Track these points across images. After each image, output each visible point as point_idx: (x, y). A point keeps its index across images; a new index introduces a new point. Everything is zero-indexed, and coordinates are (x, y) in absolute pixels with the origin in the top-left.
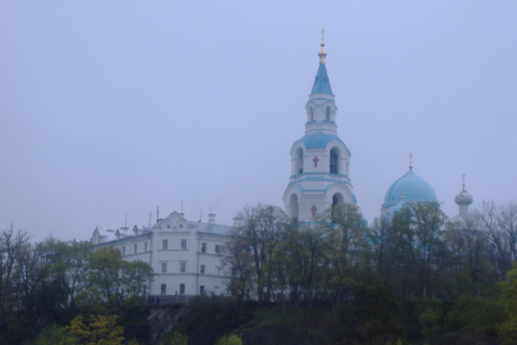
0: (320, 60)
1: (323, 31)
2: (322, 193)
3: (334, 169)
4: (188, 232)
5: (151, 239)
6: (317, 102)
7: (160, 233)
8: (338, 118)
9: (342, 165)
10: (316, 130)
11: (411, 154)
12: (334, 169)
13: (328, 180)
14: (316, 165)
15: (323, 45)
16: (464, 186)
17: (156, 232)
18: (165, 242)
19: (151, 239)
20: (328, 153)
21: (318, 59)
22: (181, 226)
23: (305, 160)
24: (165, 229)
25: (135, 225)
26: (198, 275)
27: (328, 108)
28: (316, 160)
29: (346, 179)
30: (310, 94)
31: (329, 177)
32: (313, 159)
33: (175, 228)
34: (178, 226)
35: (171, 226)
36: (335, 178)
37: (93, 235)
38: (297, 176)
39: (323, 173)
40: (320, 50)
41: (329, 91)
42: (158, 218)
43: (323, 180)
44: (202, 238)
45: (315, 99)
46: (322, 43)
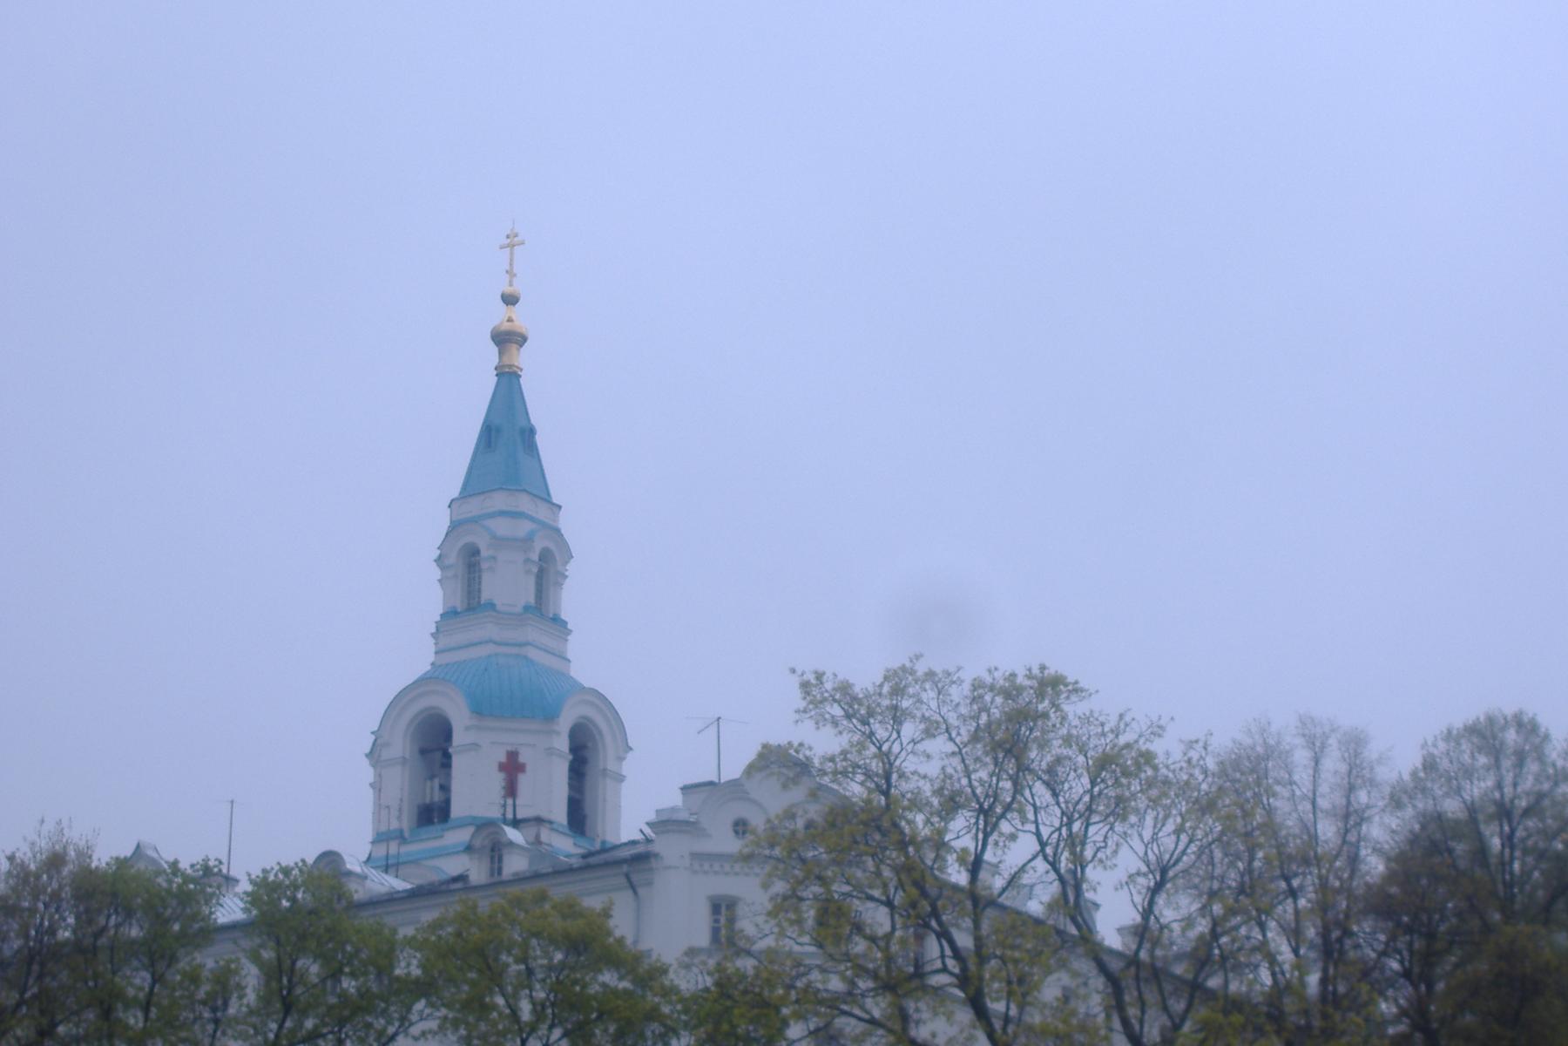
0: (497, 360)
1: (512, 242)
5: (635, 893)
6: (502, 527)
7: (696, 856)
8: (572, 601)
10: (495, 643)
15: (510, 300)
17: (671, 849)
19: (635, 893)
20: (562, 744)
21: (492, 352)
23: (460, 764)
25: (335, 848)
27: (546, 556)
28: (512, 768)
30: (455, 493)
38: (406, 834)
40: (498, 315)
42: (389, 826)
45: (492, 515)
46: (508, 290)
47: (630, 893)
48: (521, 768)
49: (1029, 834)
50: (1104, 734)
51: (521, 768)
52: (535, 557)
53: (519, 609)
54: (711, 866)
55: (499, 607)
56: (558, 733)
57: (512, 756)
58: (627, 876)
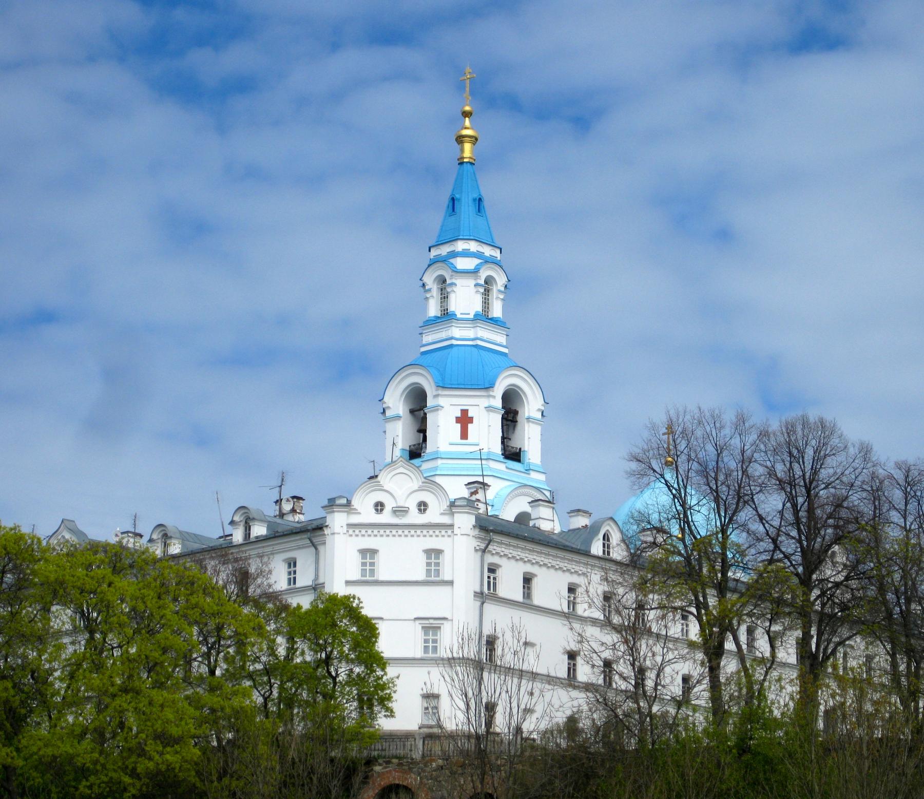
4: (451, 526)
5: (316, 549)
7: (350, 526)
14: (464, 435)
18: (368, 554)
19: (316, 549)
20: (498, 403)
22: (423, 507)
24: (367, 515)
26: (479, 666)
28: (464, 420)
32: (472, 422)
33: (400, 511)
34: (412, 505)
35: (389, 505)
37: (426, 418)
44: (490, 548)
47: (313, 549)
48: (471, 420)
49: (312, 577)
50: (73, 576)
51: (471, 420)
52: (482, 282)
53: (471, 316)
54: (373, 531)
55: (459, 316)
56: (494, 397)
57: (464, 412)
58: (310, 539)
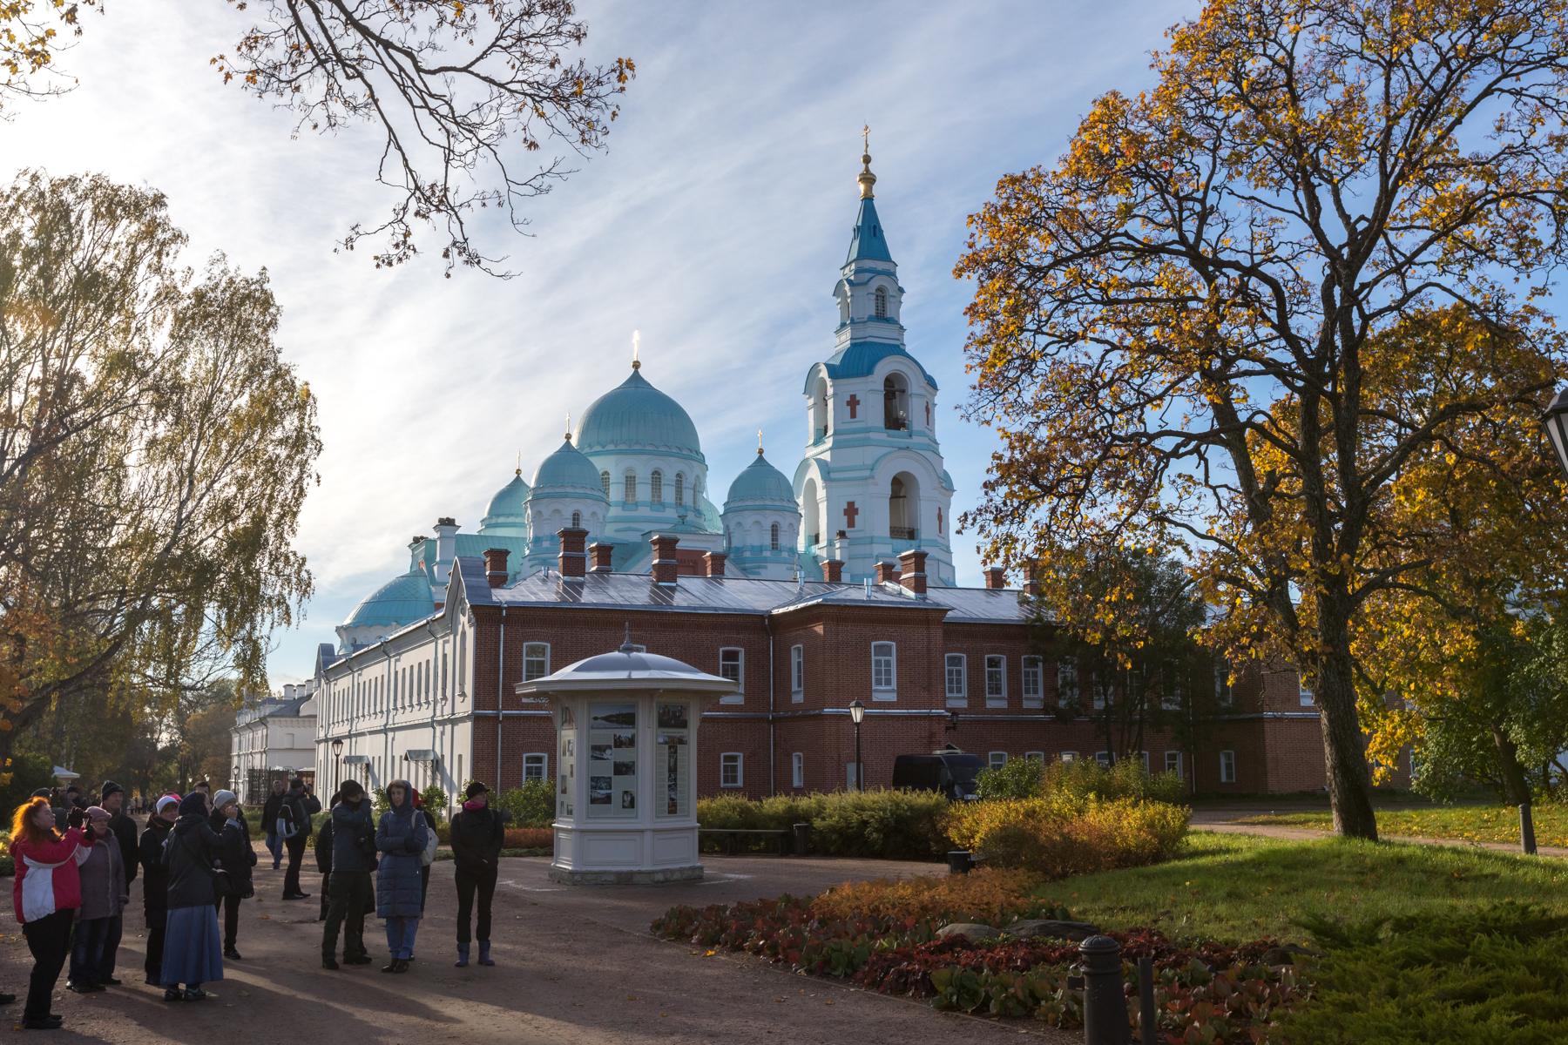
2: (867, 473)
3: (894, 422)
9: (913, 411)
11: (226, 82)
12: (894, 422)
13: (879, 444)
14: (853, 415)
16: (867, 160)
28: (853, 402)
29: (924, 440)
31: (883, 436)
36: (898, 437)
39: (868, 430)
41: (885, 256)
43: (865, 443)
48: (858, 403)
57: (853, 397)
